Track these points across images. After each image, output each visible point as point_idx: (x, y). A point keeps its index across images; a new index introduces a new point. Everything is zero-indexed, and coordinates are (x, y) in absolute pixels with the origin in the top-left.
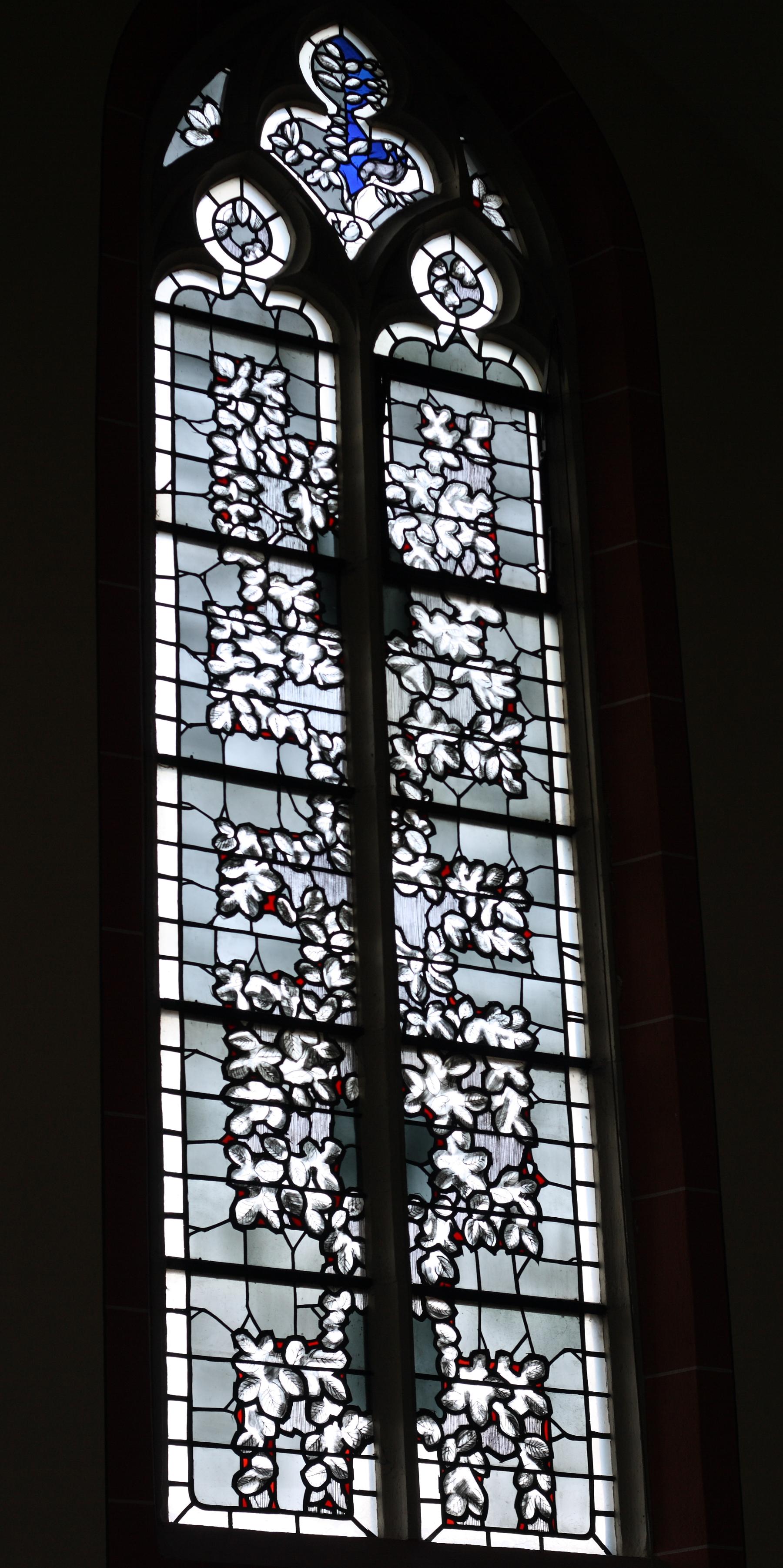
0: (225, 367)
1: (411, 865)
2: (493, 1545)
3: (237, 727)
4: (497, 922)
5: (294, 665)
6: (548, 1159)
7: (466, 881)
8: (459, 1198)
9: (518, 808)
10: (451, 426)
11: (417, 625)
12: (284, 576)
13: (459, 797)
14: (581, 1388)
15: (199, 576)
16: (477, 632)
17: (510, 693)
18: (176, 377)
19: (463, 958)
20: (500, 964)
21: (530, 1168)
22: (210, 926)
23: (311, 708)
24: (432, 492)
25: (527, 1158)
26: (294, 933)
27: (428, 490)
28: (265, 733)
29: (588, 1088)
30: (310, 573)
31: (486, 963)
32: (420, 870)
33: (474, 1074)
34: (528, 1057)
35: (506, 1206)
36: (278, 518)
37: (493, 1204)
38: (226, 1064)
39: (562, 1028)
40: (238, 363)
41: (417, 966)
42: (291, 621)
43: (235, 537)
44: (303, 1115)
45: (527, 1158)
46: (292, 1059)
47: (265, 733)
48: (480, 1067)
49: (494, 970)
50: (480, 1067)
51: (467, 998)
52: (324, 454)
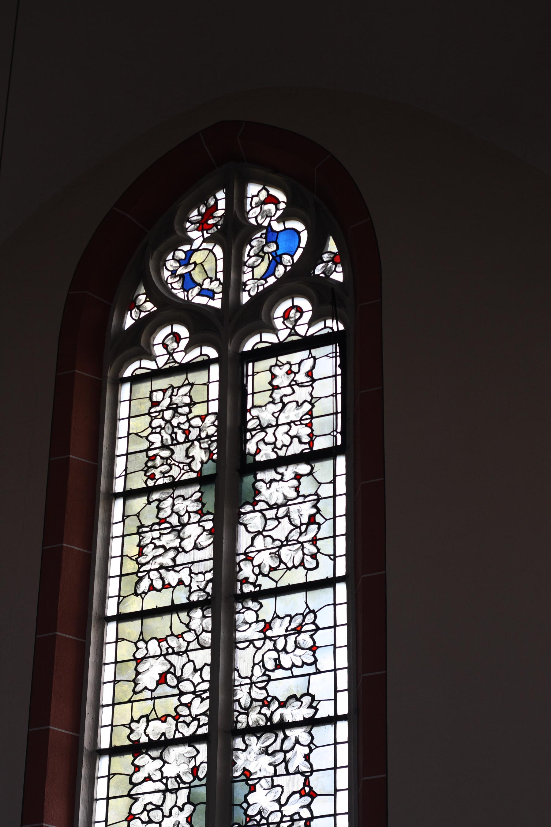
0: (157, 397)
1: (247, 632)
2: (346, 622)
3: (152, 588)
4: (297, 645)
5: (184, 544)
6: (321, 783)
7: (278, 628)
8: (262, 818)
9: (314, 576)
10: (314, 557)
11: (258, 492)
12: (183, 496)
13: (277, 582)
14: (332, 539)
15: (138, 517)
16: (295, 483)
17: (314, 511)
18: (134, 419)
19: (273, 675)
20: (296, 671)
21: (307, 789)
22: (130, 701)
23: (193, 563)
24: (274, 415)
25: (307, 783)
26: (176, 691)
27: (273, 414)
28: (166, 586)
29: (241, 493)
30: (197, 488)
31: (288, 673)
32: (253, 633)
33: (275, 744)
34: (311, 723)
35: (291, 816)
36: (181, 465)
37: (283, 816)
38: (313, 699)
39: (210, 412)
40: (164, 391)
41: (246, 688)
42: (185, 519)
43: (158, 485)
44: (172, 793)
45: (307, 783)
46: (168, 763)
47: (166, 586)
48: (281, 736)
49: (293, 677)
50: (281, 736)
51: (275, 698)
52: (210, 419)
